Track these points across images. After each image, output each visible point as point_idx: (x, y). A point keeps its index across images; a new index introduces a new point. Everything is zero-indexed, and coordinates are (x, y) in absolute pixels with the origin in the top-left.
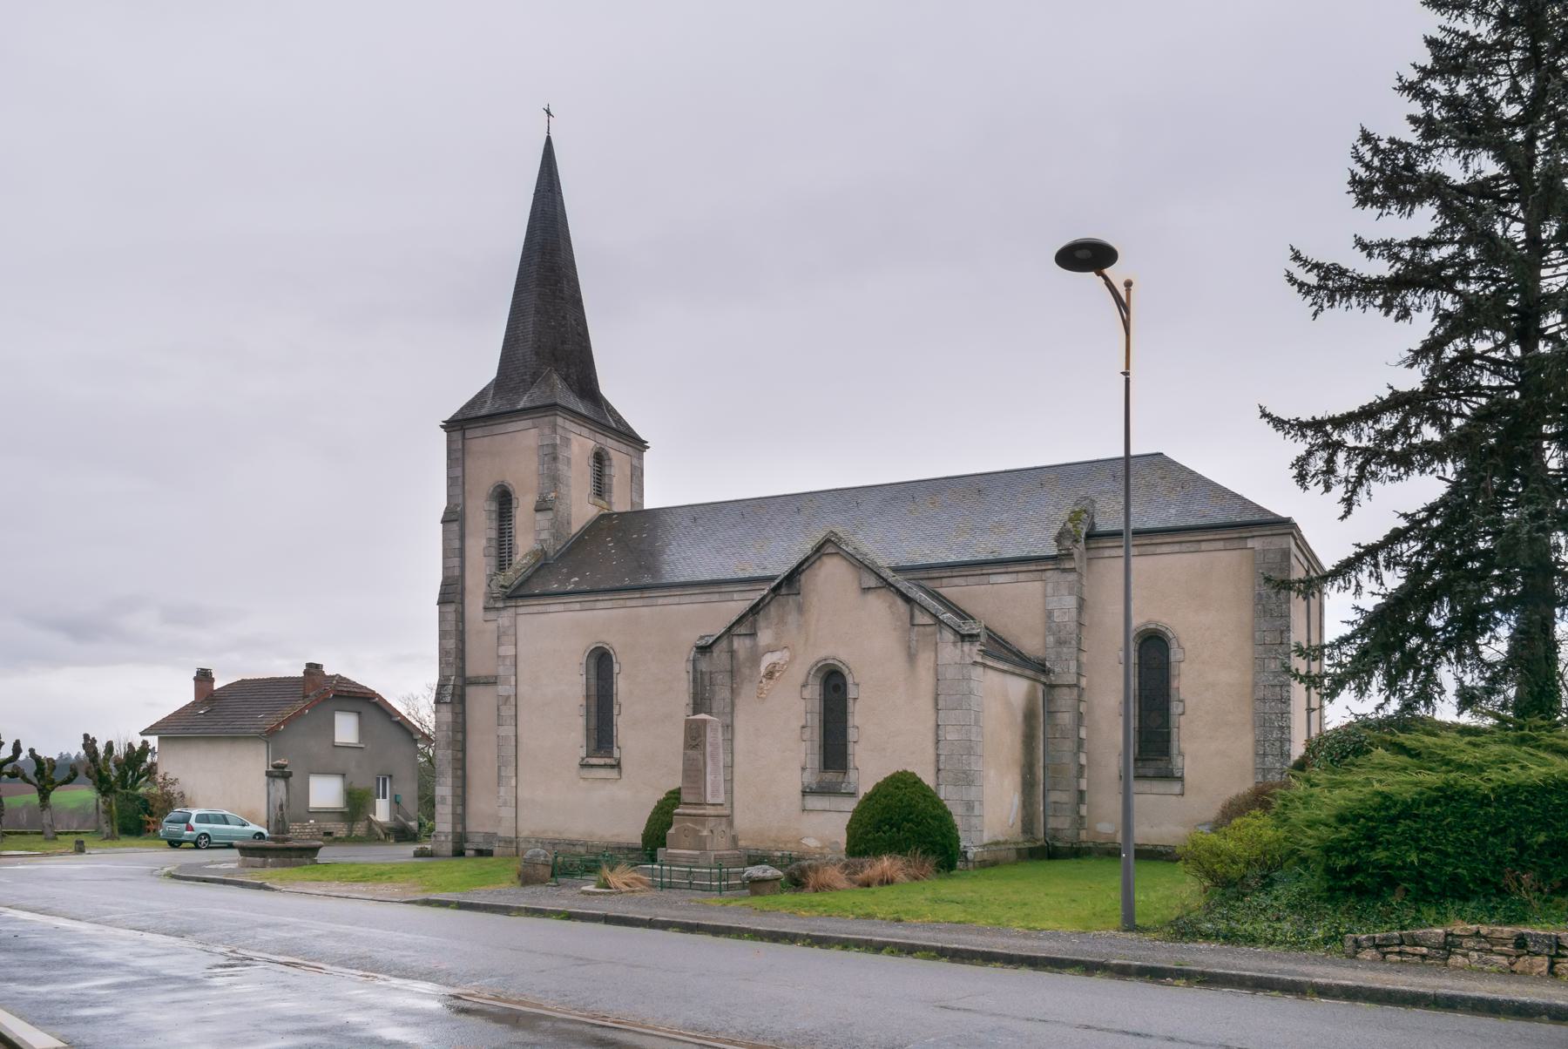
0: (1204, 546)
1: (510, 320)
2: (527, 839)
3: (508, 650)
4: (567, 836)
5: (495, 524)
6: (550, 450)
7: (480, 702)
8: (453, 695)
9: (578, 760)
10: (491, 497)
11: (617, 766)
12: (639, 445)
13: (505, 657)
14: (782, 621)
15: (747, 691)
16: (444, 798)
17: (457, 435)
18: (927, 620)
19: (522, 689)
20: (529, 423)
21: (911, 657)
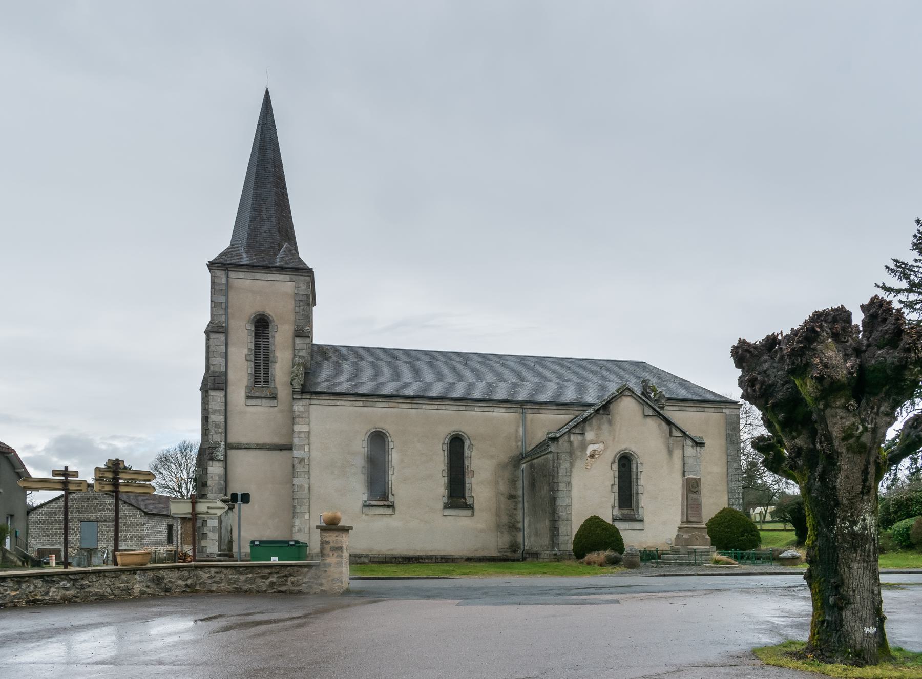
0: (706, 410)
11: (392, 506)
14: (599, 428)
15: (579, 464)
17: (220, 274)
18: (679, 434)
20: (287, 277)
21: (670, 452)
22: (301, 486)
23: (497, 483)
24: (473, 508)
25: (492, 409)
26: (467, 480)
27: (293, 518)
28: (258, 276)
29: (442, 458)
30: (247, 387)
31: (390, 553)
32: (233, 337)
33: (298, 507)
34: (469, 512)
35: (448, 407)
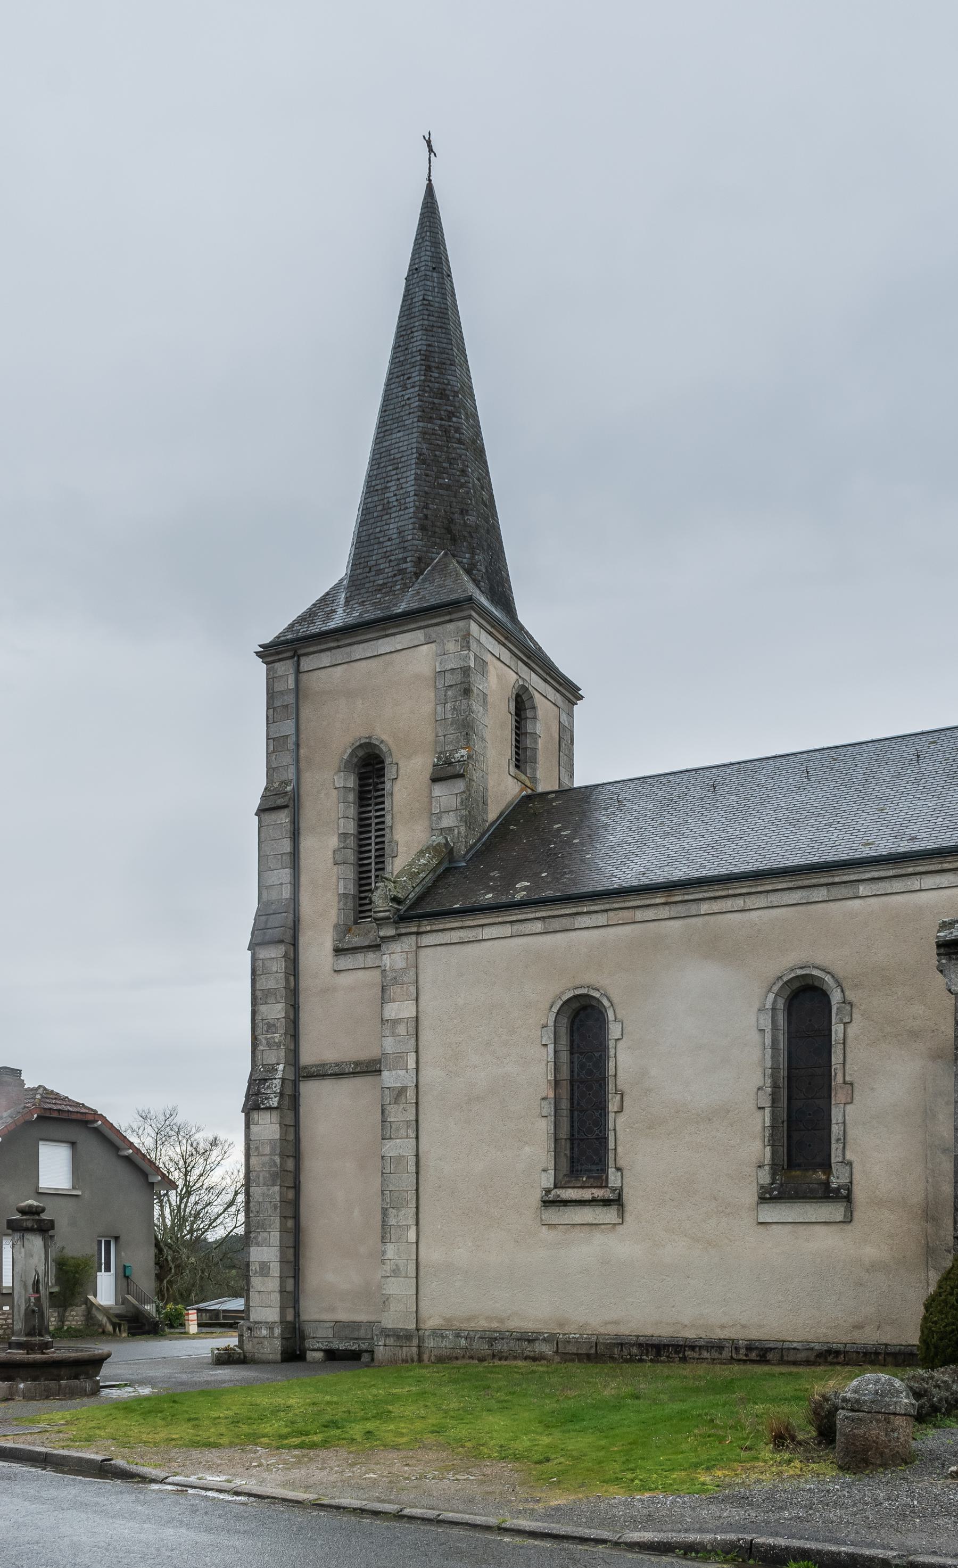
1: (371, 478)
2: (437, 1333)
3: (401, 1009)
4: (514, 1324)
5: (352, 811)
6: (458, 677)
7: (332, 1111)
8: (281, 1095)
9: (537, 1195)
10: (347, 766)
11: (616, 1201)
12: (570, 692)
13: (396, 1022)
16: (264, 1269)
17: (285, 668)
19: (427, 1074)
20: (419, 636)
22: (400, 1158)
23: (928, 1114)
24: (848, 1199)
25: (915, 883)
26: (836, 1115)
27: (383, 1240)
28: (359, 651)
29: (756, 1054)
30: (336, 926)
31: (612, 1330)
32: (309, 815)
33: (392, 1212)
34: (835, 1211)
35: (774, 899)
